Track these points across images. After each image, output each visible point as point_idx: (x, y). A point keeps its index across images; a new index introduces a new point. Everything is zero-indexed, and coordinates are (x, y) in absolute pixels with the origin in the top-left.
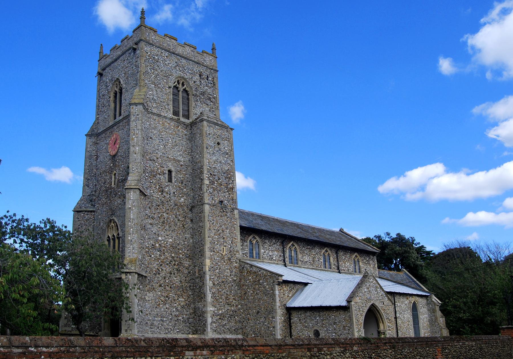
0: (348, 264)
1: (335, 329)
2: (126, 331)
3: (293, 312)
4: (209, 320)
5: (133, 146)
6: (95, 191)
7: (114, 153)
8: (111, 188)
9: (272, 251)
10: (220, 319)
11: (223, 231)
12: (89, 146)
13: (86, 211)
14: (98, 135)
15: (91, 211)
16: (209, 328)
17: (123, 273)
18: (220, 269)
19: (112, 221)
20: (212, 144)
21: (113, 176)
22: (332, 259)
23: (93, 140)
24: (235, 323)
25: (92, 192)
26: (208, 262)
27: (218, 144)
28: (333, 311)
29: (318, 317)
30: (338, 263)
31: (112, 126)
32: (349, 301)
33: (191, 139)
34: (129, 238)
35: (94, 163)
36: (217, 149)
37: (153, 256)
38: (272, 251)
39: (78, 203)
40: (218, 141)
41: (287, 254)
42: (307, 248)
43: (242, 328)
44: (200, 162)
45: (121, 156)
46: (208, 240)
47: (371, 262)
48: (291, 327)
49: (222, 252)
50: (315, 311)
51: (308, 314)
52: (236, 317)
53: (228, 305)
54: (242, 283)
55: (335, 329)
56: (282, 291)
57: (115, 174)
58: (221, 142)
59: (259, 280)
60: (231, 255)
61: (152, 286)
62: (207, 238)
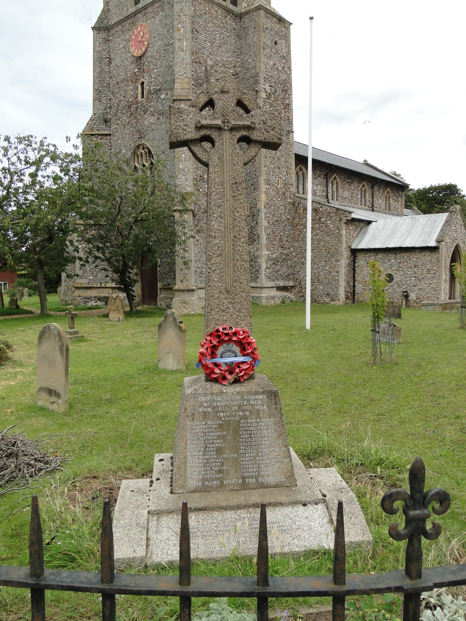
0: (380, 201)
1: (415, 273)
2: (182, 281)
3: (359, 254)
4: (264, 266)
5: (179, 40)
6: (111, 108)
7: (140, 53)
8: (137, 103)
9: (316, 185)
10: (274, 264)
11: (278, 159)
12: (97, 44)
13: (99, 135)
14: (108, 29)
15: (106, 135)
16: (263, 275)
17: (175, 211)
18: (275, 205)
19: (141, 147)
20: (268, 42)
21: (140, 87)
22: (367, 194)
23: (103, 35)
24: (288, 268)
25: (105, 109)
26: (263, 197)
27: (276, 43)
28: (416, 252)
29: (393, 259)
30: (373, 200)
31: (135, 14)
32: (438, 241)
33: (240, 36)
34: (181, 167)
35: (106, 69)
36: (274, 50)
37: (201, 190)
38: (316, 185)
39: (88, 124)
40: (276, 39)
41: (330, 190)
42: (347, 182)
43: (293, 274)
44: (254, 67)
45: (151, 57)
46: (264, 170)
47: (400, 199)
48: (354, 271)
49: (277, 185)
50: (391, 253)
51: (380, 256)
52: (288, 261)
53: (282, 247)
54: (295, 221)
55: (415, 273)
56: (348, 230)
57: (142, 84)
58: (279, 42)
59: (320, 218)
60: (285, 189)
61: (201, 226)
62: (263, 168)
